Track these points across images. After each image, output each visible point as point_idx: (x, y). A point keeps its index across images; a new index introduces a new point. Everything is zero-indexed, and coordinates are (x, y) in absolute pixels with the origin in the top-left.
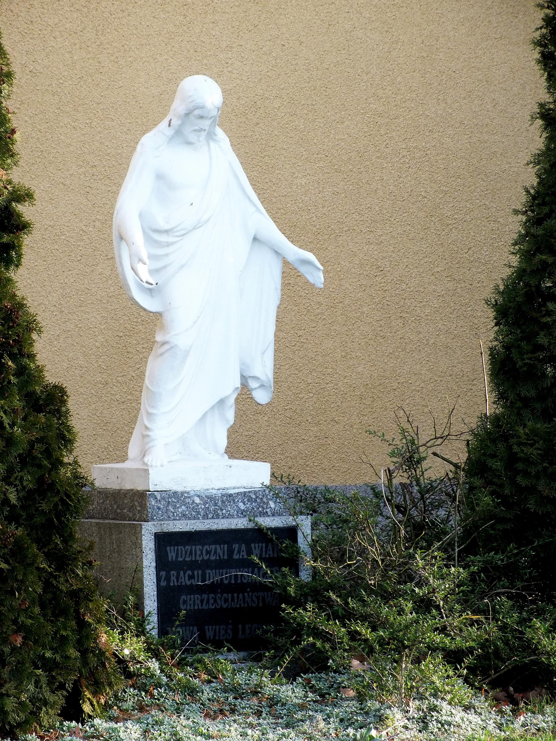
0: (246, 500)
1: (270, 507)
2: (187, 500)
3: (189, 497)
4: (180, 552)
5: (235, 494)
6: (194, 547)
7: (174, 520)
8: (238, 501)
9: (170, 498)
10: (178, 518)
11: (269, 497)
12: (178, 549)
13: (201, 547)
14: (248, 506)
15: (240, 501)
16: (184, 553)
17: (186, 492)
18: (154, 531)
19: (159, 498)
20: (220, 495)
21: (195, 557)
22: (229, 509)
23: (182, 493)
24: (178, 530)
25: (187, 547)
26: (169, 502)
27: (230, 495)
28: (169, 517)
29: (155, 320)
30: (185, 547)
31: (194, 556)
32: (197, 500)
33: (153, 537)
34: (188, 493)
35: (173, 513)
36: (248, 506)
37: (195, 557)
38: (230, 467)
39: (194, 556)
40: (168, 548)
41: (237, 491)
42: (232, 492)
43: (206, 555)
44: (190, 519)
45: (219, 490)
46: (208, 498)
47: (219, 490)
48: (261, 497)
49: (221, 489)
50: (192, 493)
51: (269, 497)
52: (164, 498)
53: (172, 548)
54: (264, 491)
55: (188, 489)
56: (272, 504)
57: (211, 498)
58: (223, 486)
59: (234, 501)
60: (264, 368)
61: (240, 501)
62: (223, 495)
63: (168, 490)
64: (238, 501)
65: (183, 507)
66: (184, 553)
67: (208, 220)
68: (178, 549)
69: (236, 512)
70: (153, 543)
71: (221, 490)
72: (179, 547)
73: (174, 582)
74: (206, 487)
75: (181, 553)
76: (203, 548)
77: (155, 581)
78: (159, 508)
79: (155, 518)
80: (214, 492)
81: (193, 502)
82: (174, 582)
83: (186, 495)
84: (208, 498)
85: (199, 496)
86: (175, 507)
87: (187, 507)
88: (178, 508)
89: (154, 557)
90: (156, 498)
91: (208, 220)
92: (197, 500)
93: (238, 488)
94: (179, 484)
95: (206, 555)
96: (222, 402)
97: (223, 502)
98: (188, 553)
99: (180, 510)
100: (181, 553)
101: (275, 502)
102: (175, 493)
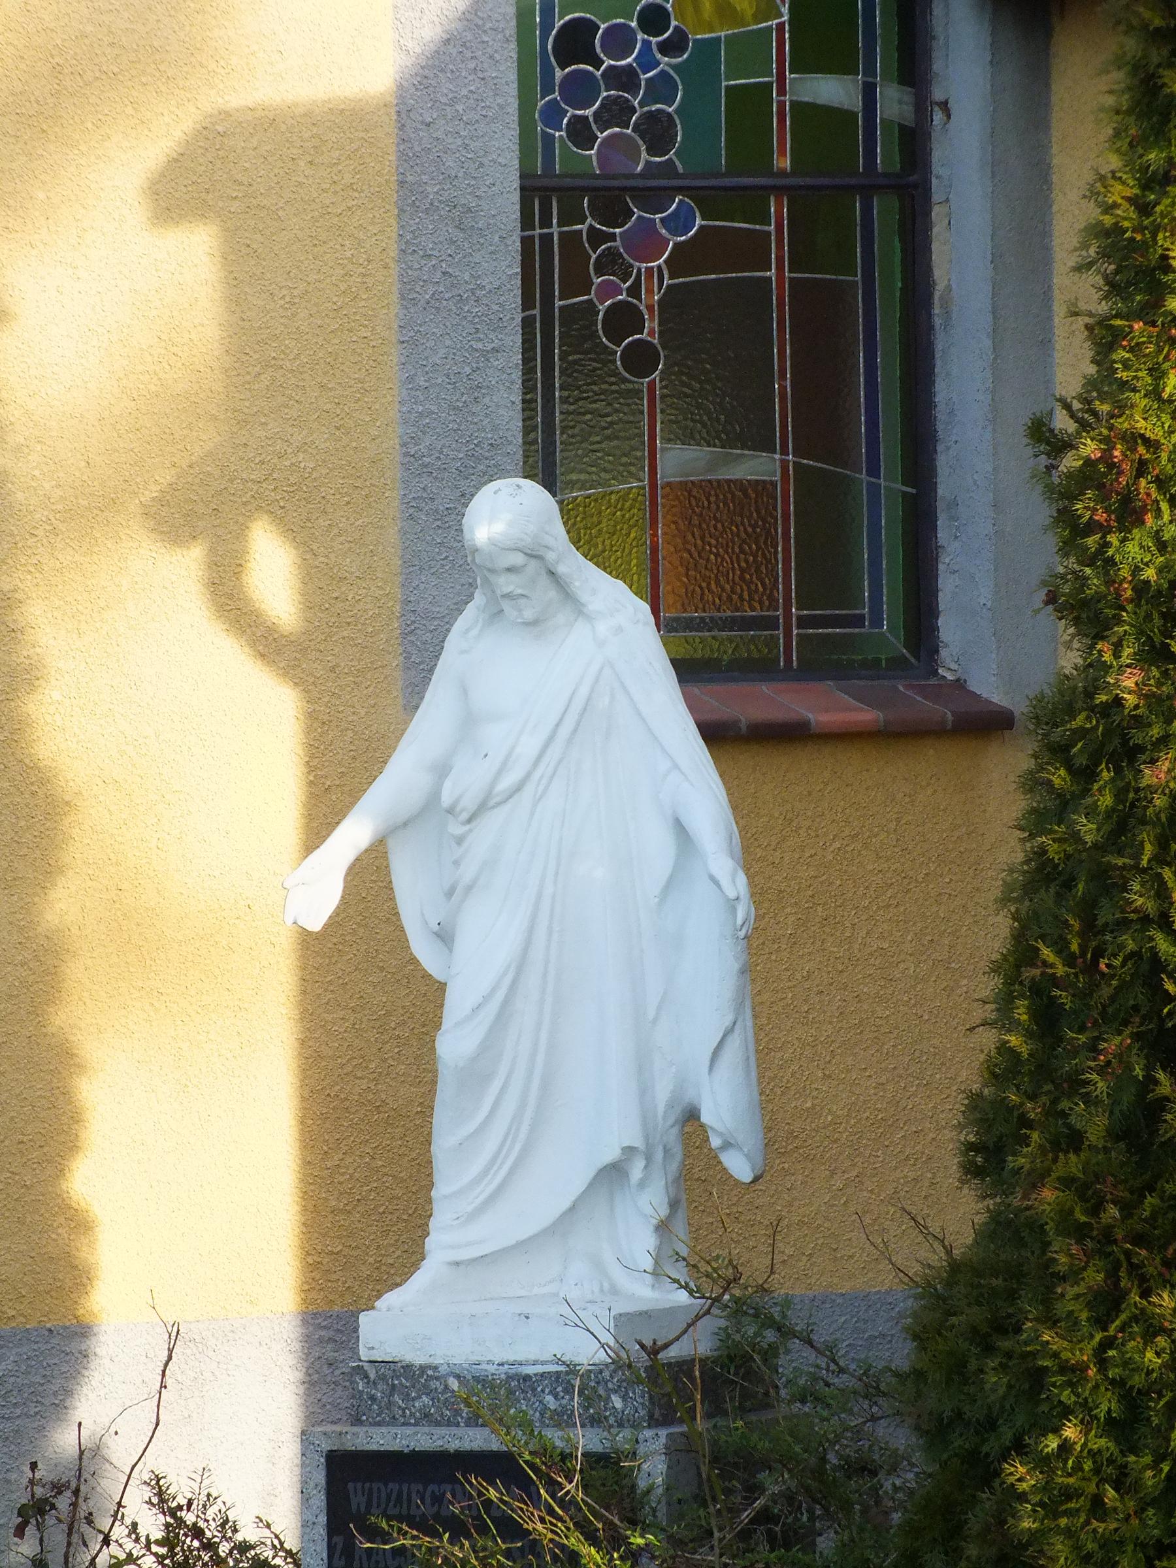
0: (560, 1389)
1: (614, 1407)
2: (434, 1384)
3: (437, 1378)
4: (375, 1495)
5: (535, 1375)
6: (405, 1487)
7: (404, 1424)
8: (543, 1391)
9: (398, 1378)
10: (413, 1421)
11: (610, 1385)
12: (371, 1489)
13: (420, 1487)
14: (564, 1402)
15: (547, 1391)
16: (384, 1495)
17: (430, 1367)
18: (326, 1446)
19: (372, 1376)
20: (503, 1376)
21: (409, 1509)
22: (524, 1408)
23: (423, 1369)
24: (374, 1447)
25: (391, 1485)
26: (393, 1385)
27: (527, 1378)
28: (394, 1417)
29: (442, 987)
30: (386, 1485)
31: (405, 1506)
32: (454, 1384)
33: (322, 1460)
34: (435, 1368)
35: (404, 1410)
36: (564, 1402)
37: (409, 1509)
38: (527, 1318)
39: (405, 1506)
40: (351, 1486)
41: (540, 1369)
42: (530, 1370)
43: (433, 1505)
44: (438, 1424)
45: (502, 1365)
46: (478, 1382)
47: (502, 1365)
48: (593, 1384)
49: (507, 1363)
50: (443, 1370)
51: (610, 1385)
52: (383, 1378)
53: (359, 1485)
54: (601, 1372)
55: (438, 1361)
56: (617, 1402)
57: (482, 1380)
58: (511, 1358)
59: (534, 1390)
60: (726, 1105)
61: (547, 1391)
62: (510, 1377)
63: (397, 1359)
64: (543, 1391)
65: (424, 1397)
66: (384, 1495)
67: (518, 788)
68: (371, 1489)
69: (538, 1414)
70: (324, 1473)
71: (506, 1366)
72: (375, 1486)
73: (360, 1559)
74: (474, 1358)
75: (379, 1498)
76: (425, 1489)
77: (325, 1555)
78: (373, 1398)
79: (364, 1418)
80: (492, 1369)
81: (446, 1387)
82: (360, 1559)
83: (430, 1372)
84: (478, 1382)
85: (458, 1377)
86: (407, 1397)
87: (432, 1399)
88: (414, 1399)
89: (324, 1504)
90: (367, 1377)
91: (518, 788)
92: (454, 1384)
93: (543, 1363)
94: (419, 1349)
95: (433, 1505)
96: (612, 1175)
97: (511, 1392)
98: (394, 1497)
99: (417, 1405)
100: (379, 1498)
101: (624, 1398)
102: (408, 1367)
